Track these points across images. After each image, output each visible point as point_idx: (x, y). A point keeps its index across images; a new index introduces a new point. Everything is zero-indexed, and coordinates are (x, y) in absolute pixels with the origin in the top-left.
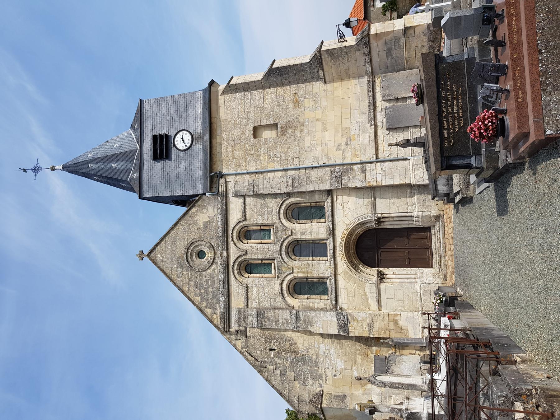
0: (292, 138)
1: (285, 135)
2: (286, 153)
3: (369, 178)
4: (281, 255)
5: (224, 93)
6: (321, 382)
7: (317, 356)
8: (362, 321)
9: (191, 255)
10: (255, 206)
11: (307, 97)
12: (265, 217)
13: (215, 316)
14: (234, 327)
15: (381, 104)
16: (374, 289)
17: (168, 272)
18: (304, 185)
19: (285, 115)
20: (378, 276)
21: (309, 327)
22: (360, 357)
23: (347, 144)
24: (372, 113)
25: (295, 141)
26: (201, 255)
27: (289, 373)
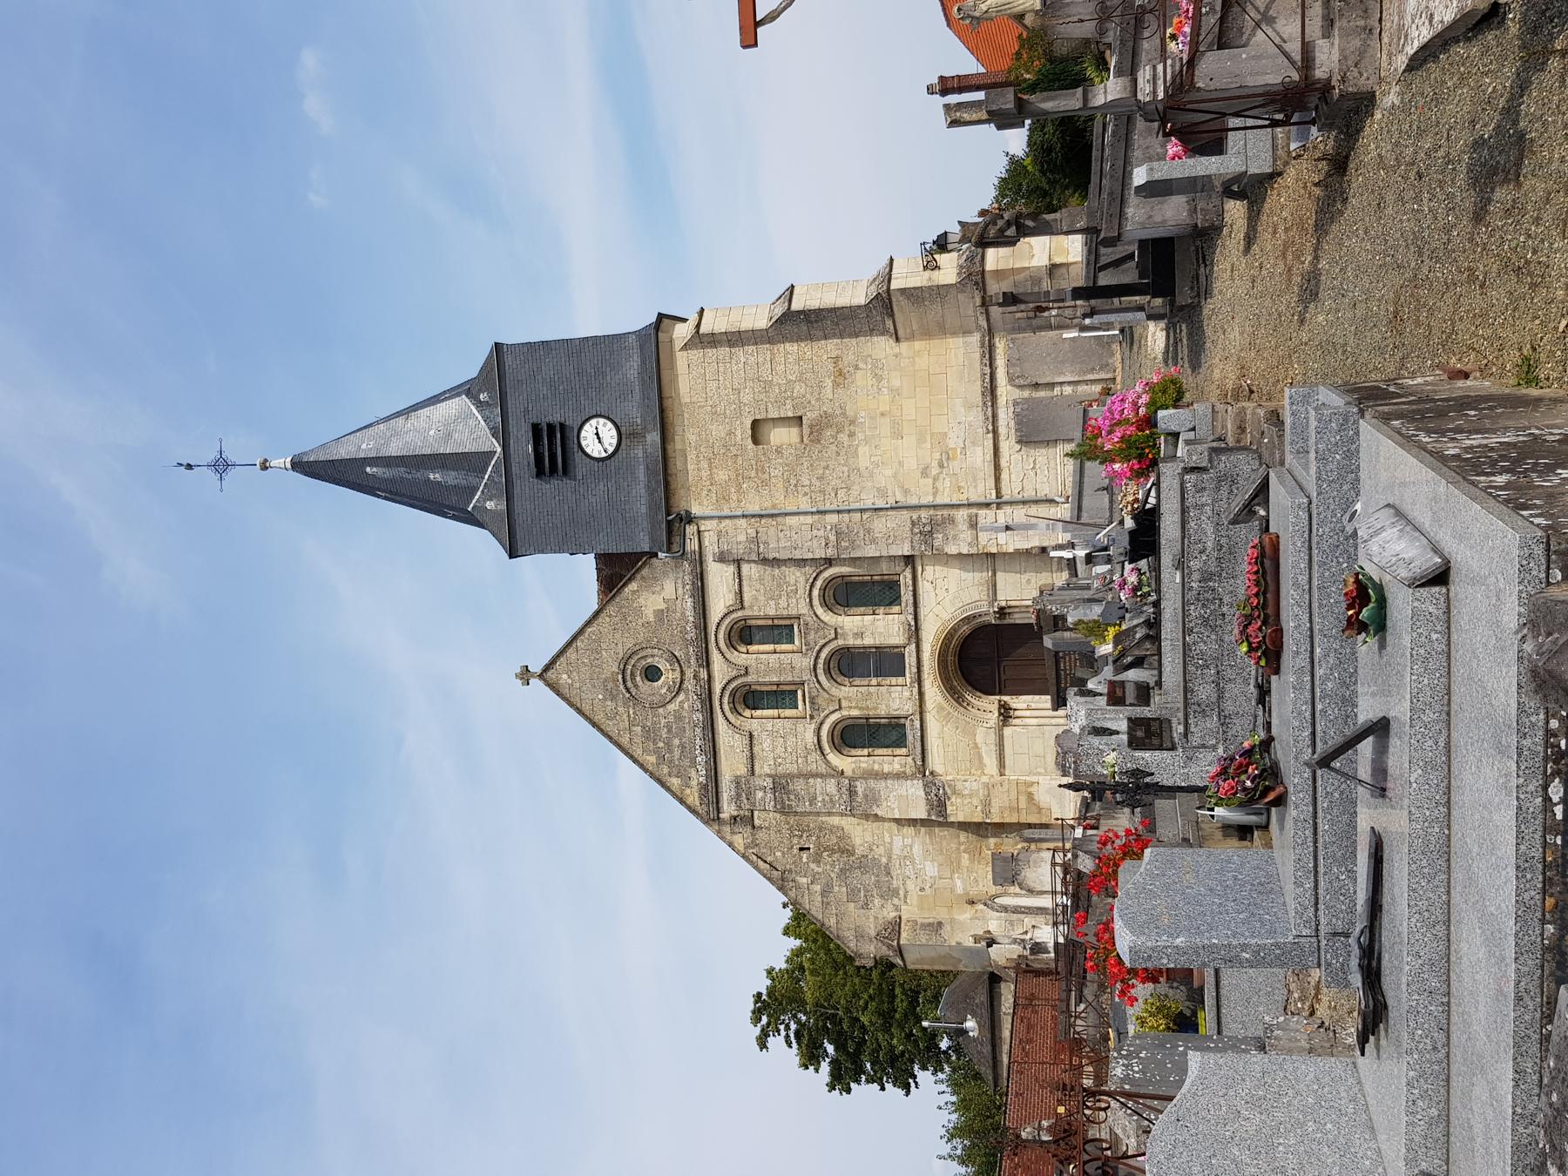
2: (820, 478)
5: (685, 347)
6: (896, 901)
7: (890, 858)
8: (971, 796)
9: (632, 674)
10: (761, 579)
11: (861, 365)
12: (783, 603)
13: (688, 791)
14: (728, 809)
15: (1005, 391)
16: (992, 738)
17: (586, 708)
19: (818, 400)
23: (941, 466)
25: (838, 454)
26: (652, 674)
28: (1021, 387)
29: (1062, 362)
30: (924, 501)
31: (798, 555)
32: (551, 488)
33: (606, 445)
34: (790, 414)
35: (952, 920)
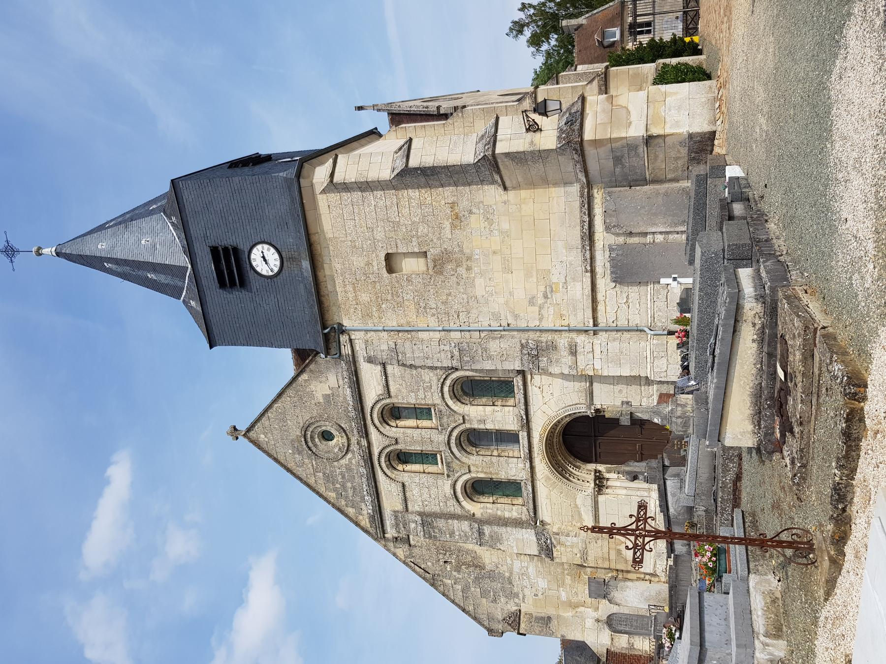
0: (454, 279)
1: (441, 273)
2: (445, 303)
3: (581, 365)
4: (450, 448)
5: (324, 191)
6: (516, 600)
7: (511, 573)
8: (572, 547)
9: (312, 437)
10: (402, 377)
11: (474, 210)
12: (421, 394)
13: (361, 517)
14: (391, 533)
15: (601, 236)
16: (589, 502)
17: (281, 458)
18: (478, 361)
19: (439, 239)
20: (595, 484)
21: (498, 544)
22: (569, 577)
23: (546, 297)
24: (588, 252)
25: (458, 284)
26: (327, 436)
27: (473, 589)
28: (617, 235)
29: (655, 214)
30: (532, 325)
31: (429, 363)
32: (236, 296)
33: (272, 266)
34: (416, 250)
35: (558, 617)
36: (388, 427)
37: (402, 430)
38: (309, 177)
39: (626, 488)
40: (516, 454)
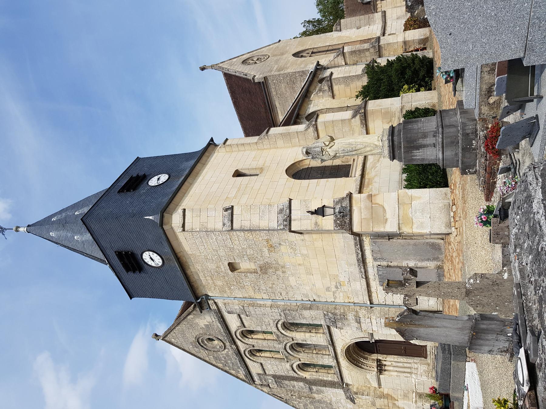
1: (266, 273)
14: (258, 382)
17: (187, 349)
20: (378, 369)
23: (337, 287)
36: (247, 339)
37: (256, 341)
38: (169, 222)
39: (397, 371)
40: (327, 353)
